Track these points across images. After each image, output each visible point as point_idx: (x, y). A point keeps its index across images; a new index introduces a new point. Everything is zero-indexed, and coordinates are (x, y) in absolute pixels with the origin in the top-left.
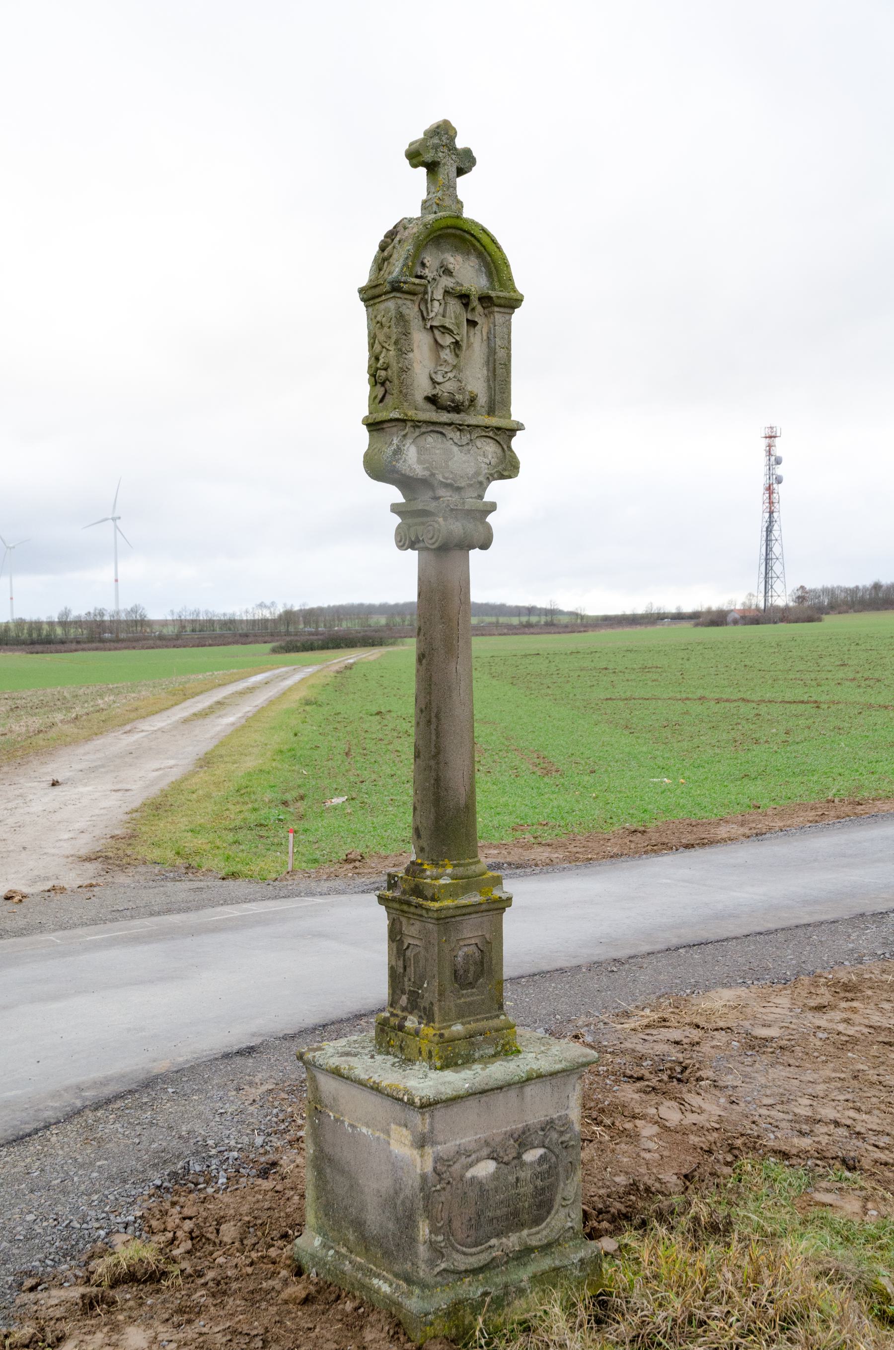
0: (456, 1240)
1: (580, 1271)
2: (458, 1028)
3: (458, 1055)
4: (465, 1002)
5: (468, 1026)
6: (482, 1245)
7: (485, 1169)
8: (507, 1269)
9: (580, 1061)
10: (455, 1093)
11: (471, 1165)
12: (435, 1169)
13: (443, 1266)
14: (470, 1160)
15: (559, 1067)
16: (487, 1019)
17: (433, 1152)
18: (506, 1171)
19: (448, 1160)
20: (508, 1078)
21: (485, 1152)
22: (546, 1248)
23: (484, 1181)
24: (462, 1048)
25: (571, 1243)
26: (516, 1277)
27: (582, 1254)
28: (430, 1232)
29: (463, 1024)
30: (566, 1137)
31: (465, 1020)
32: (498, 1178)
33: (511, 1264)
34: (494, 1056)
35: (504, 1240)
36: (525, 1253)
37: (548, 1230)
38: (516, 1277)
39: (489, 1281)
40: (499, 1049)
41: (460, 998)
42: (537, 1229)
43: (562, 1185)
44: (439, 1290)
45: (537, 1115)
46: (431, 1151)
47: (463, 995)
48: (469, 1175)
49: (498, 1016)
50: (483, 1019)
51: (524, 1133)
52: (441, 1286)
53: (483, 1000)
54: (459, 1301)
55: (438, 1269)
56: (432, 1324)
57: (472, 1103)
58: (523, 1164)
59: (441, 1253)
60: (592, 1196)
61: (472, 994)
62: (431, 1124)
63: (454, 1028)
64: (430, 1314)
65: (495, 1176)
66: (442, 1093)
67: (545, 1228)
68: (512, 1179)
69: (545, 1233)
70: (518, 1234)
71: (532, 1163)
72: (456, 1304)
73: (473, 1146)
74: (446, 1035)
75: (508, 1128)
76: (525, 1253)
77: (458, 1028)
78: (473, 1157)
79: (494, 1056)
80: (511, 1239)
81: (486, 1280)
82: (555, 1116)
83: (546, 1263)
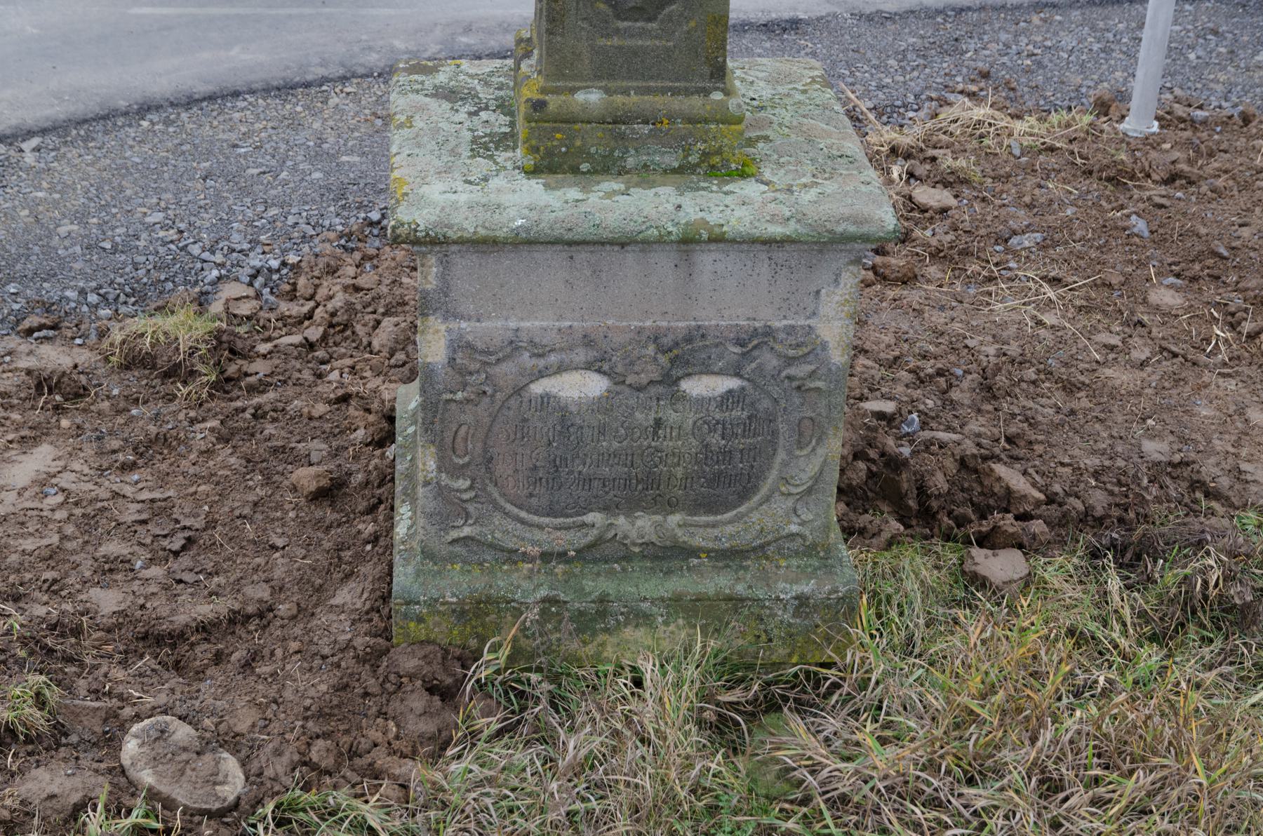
0: (503, 495)
1: (793, 616)
2: (591, 98)
3: (584, 153)
4: (620, 48)
5: (619, 99)
6: (567, 516)
7: (580, 387)
8: (624, 570)
9: (840, 229)
10: (482, 232)
11: (541, 375)
12: (452, 360)
13: (467, 531)
14: (541, 363)
15: (777, 230)
16: (675, 92)
17: (449, 331)
18: (632, 402)
19: (488, 353)
20: (632, 227)
21: (581, 355)
22: (731, 556)
23: (574, 409)
24: (595, 141)
25: (794, 562)
26: (633, 590)
27: (806, 588)
28: (439, 469)
29: (607, 91)
30: (800, 370)
31: (612, 85)
32: (607, 411)
33: (637, 565)
34: (675, 171)
35: (621, 521)
36: (670, 555)
37: (739, 527)
38: (633, 590)
39: (572, 582)
40: (693, 159)
41: (608, 36)
42: (711, 518)
43: (781, 455)
44: (458, 567)
45: (726, 313)
46: (443, 327)
47: (617, 31)
48: (538, 388)
49: (706, 92)
50: (663, 91)
51: (689, 339)
52: (464, 562)
53: (667, 49)
54: (489, 597)
55: (455, 534)
56: (420, 620)
57: (554, 259)
58: (678, 398)
59: (465, 509)
60: (1062, 464)
61: (643, 33)
62: (443, 277)
63: (580, 97)
64: (418, 603)
65: (602, 405)
66: (450, 226)
67: (730, 522)
68: (643, 418)
69: (729, 529)
70: (658, 518)
71: (701, 402)
72: (479, 602)
73: (550, 338)
74: (552, 107)
75: (648, 323)
76: (670, 555)
77: (591, 98)
78: (553, 358)
79: (675, 171)
80: (639, 523)
81: (569, 575)
82: (777, 324)
83: (717, 582)
